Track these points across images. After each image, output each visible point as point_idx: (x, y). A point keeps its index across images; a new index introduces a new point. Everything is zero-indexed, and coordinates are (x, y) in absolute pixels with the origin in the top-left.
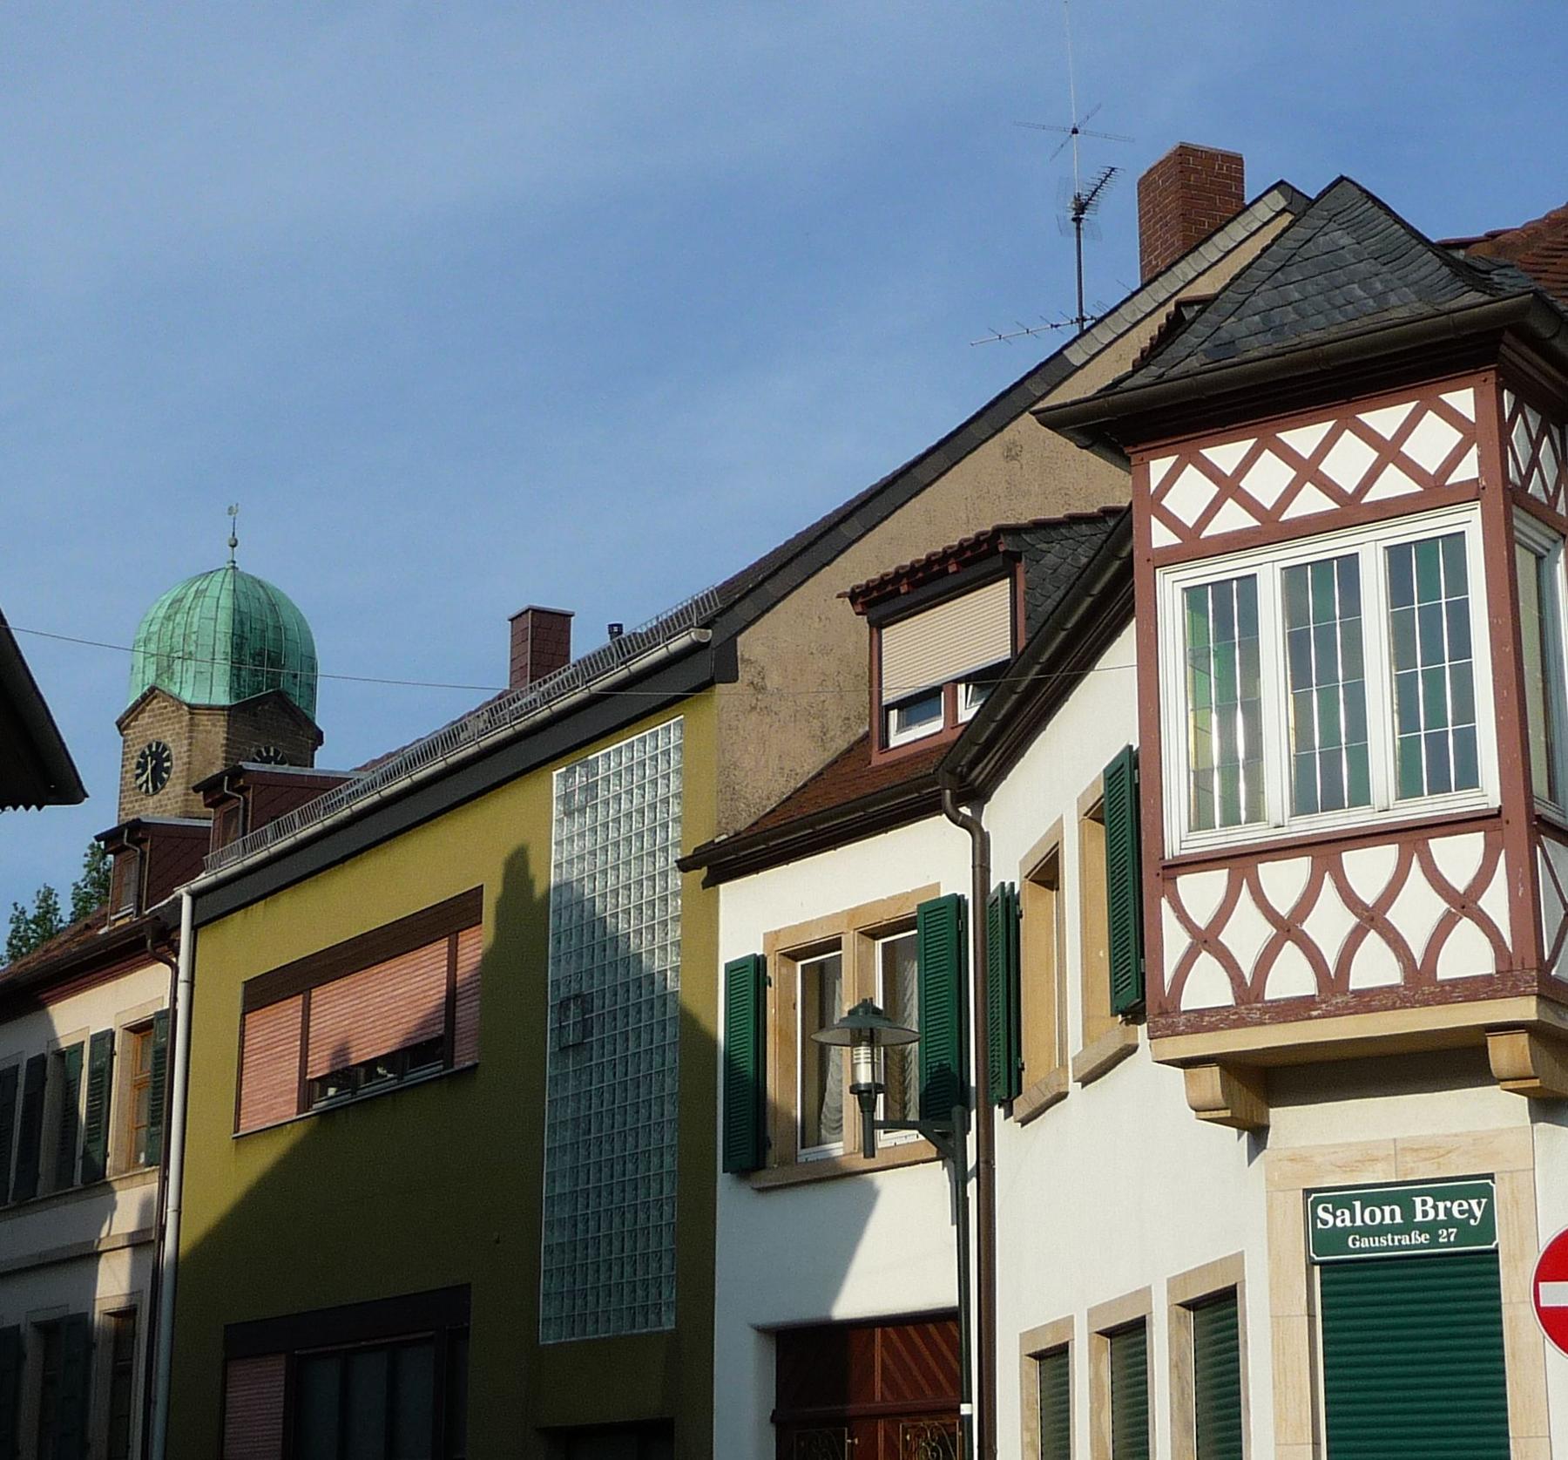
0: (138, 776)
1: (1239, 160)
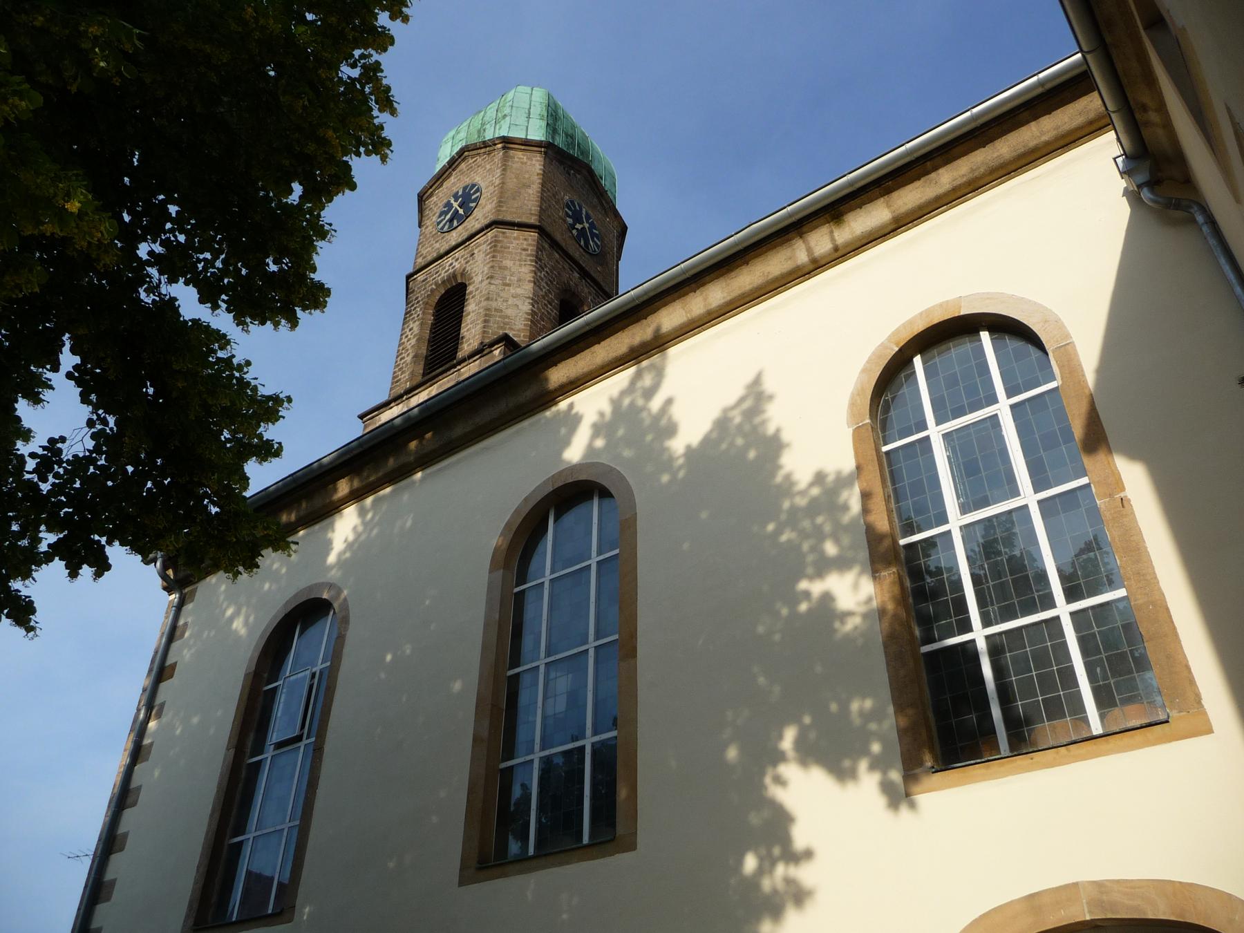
0: (439, 223)
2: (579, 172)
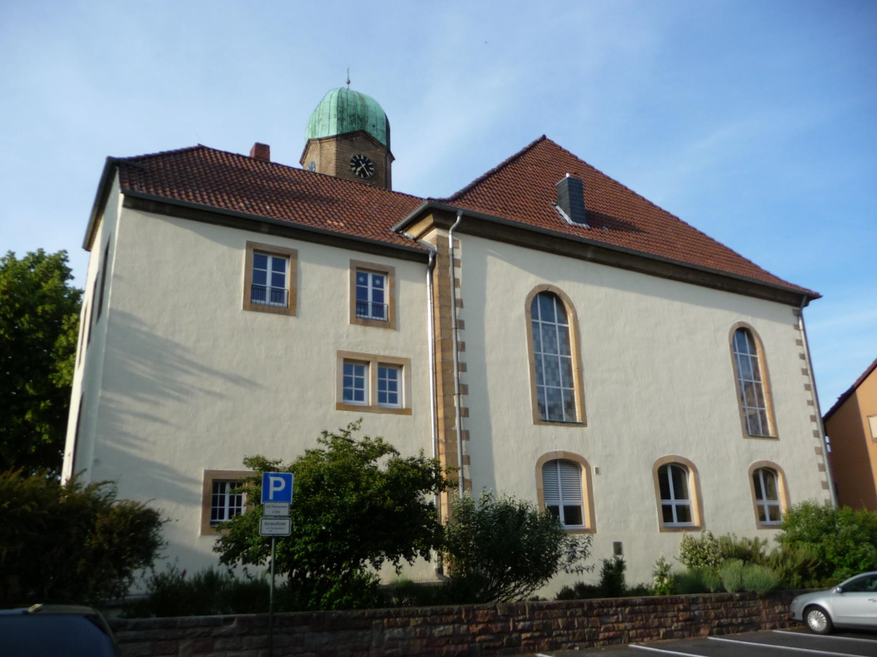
2: (358, 136)
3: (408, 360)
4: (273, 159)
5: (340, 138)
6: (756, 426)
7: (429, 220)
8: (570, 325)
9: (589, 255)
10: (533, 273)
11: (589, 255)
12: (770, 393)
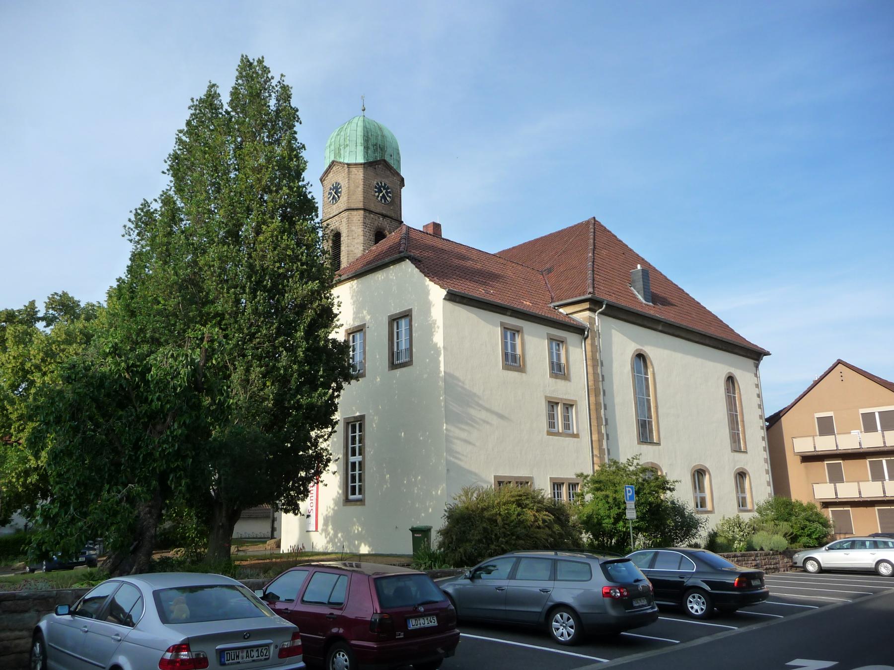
1: (595, 222)
3: (576, 401)
4: (444, 235)
5: (368, 165)
6: (737, 444)
7: (586, 305)
8: (650, 376)
9: (660, 328)
10: (633, 341)
11: (660, 328)
12: (743, 421)
